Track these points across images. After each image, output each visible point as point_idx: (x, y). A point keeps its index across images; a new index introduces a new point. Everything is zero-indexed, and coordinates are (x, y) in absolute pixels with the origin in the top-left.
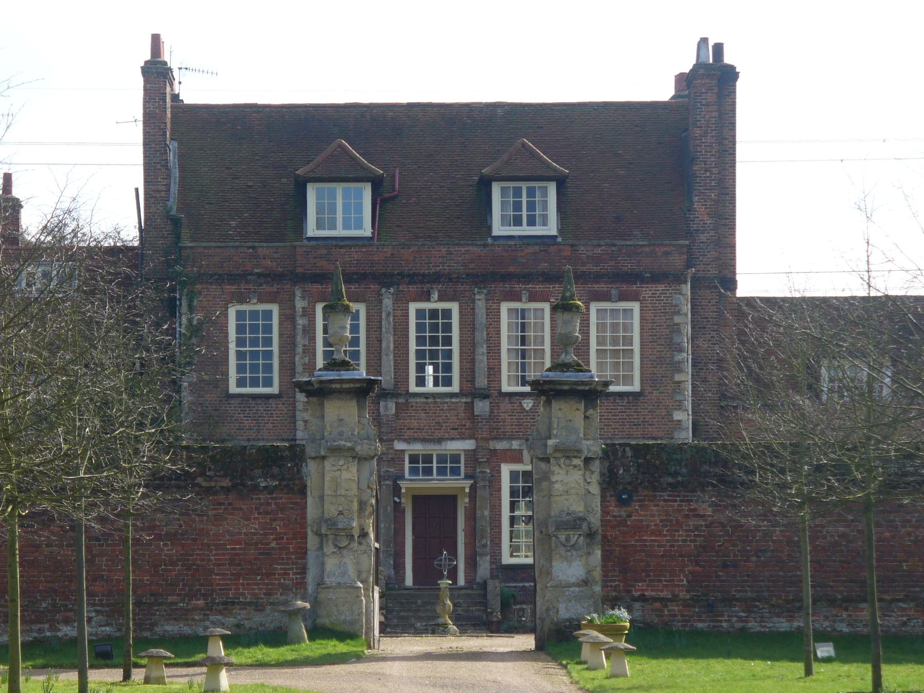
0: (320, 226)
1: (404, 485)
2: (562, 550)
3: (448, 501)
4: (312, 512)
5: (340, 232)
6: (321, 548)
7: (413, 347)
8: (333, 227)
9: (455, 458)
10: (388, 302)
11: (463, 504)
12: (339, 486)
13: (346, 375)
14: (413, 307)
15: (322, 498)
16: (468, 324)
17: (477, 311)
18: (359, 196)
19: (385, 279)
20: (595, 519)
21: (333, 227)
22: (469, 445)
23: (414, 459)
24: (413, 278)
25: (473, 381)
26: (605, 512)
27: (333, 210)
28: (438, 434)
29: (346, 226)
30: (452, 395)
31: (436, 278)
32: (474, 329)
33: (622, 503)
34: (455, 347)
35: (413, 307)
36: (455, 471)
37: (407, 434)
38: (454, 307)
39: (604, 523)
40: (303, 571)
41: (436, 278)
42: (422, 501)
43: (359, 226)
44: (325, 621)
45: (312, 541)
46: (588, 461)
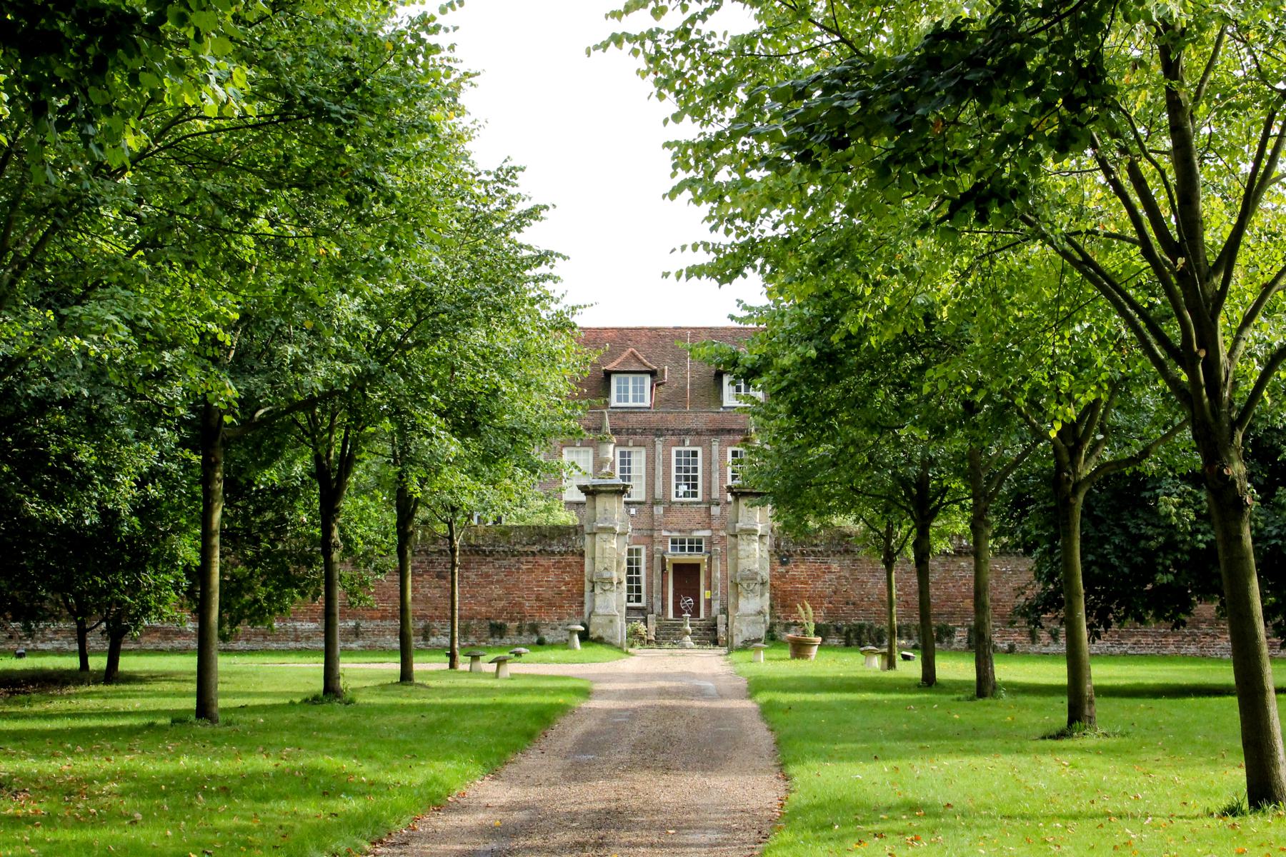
0: (619, 400)
1: (667, 557)
2: (744, 593)
3: (695, 568)
4: (587, 568)
5: (631, 404)
6: (593, 591)
7: (674, 473)
8: (627, 401)
9: (699, 542)
10: (659, 447)
11: (704, 568)
12: (609, 554)
13: (609, 482)
14: (674, 450)
15: (593, 559)
16: (708, 461)
17: (1015, 756)
18: (643, 382)
19: (659, 432)
20: (766, 574)
21: (627, 401)
22: (707, 533)
23: (674, 542)
24: (675, 432)
25: (710, 495)
26: (772, 569)
27: (626, 390)
28: (688, 527)
29: (635, 400)
30: (698, 503)
31: (687, 432)
32: (711, 464)
33: (783, 564)
34: (699, 474)
35: (674, 450)
36: (699, 549)
37: (670, 527)
38: (699, 450)
39: (772, 576)
40: (582, 603)
41: (687, 432)
42: (678, 568)
43: (642, 400)
44: (319, 686)
45: (587, 587)
46: (761, 536)
